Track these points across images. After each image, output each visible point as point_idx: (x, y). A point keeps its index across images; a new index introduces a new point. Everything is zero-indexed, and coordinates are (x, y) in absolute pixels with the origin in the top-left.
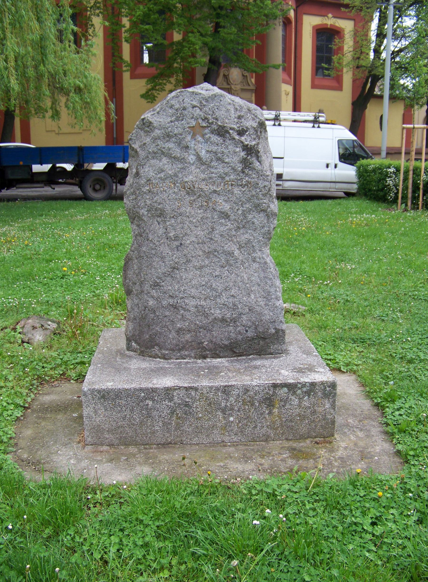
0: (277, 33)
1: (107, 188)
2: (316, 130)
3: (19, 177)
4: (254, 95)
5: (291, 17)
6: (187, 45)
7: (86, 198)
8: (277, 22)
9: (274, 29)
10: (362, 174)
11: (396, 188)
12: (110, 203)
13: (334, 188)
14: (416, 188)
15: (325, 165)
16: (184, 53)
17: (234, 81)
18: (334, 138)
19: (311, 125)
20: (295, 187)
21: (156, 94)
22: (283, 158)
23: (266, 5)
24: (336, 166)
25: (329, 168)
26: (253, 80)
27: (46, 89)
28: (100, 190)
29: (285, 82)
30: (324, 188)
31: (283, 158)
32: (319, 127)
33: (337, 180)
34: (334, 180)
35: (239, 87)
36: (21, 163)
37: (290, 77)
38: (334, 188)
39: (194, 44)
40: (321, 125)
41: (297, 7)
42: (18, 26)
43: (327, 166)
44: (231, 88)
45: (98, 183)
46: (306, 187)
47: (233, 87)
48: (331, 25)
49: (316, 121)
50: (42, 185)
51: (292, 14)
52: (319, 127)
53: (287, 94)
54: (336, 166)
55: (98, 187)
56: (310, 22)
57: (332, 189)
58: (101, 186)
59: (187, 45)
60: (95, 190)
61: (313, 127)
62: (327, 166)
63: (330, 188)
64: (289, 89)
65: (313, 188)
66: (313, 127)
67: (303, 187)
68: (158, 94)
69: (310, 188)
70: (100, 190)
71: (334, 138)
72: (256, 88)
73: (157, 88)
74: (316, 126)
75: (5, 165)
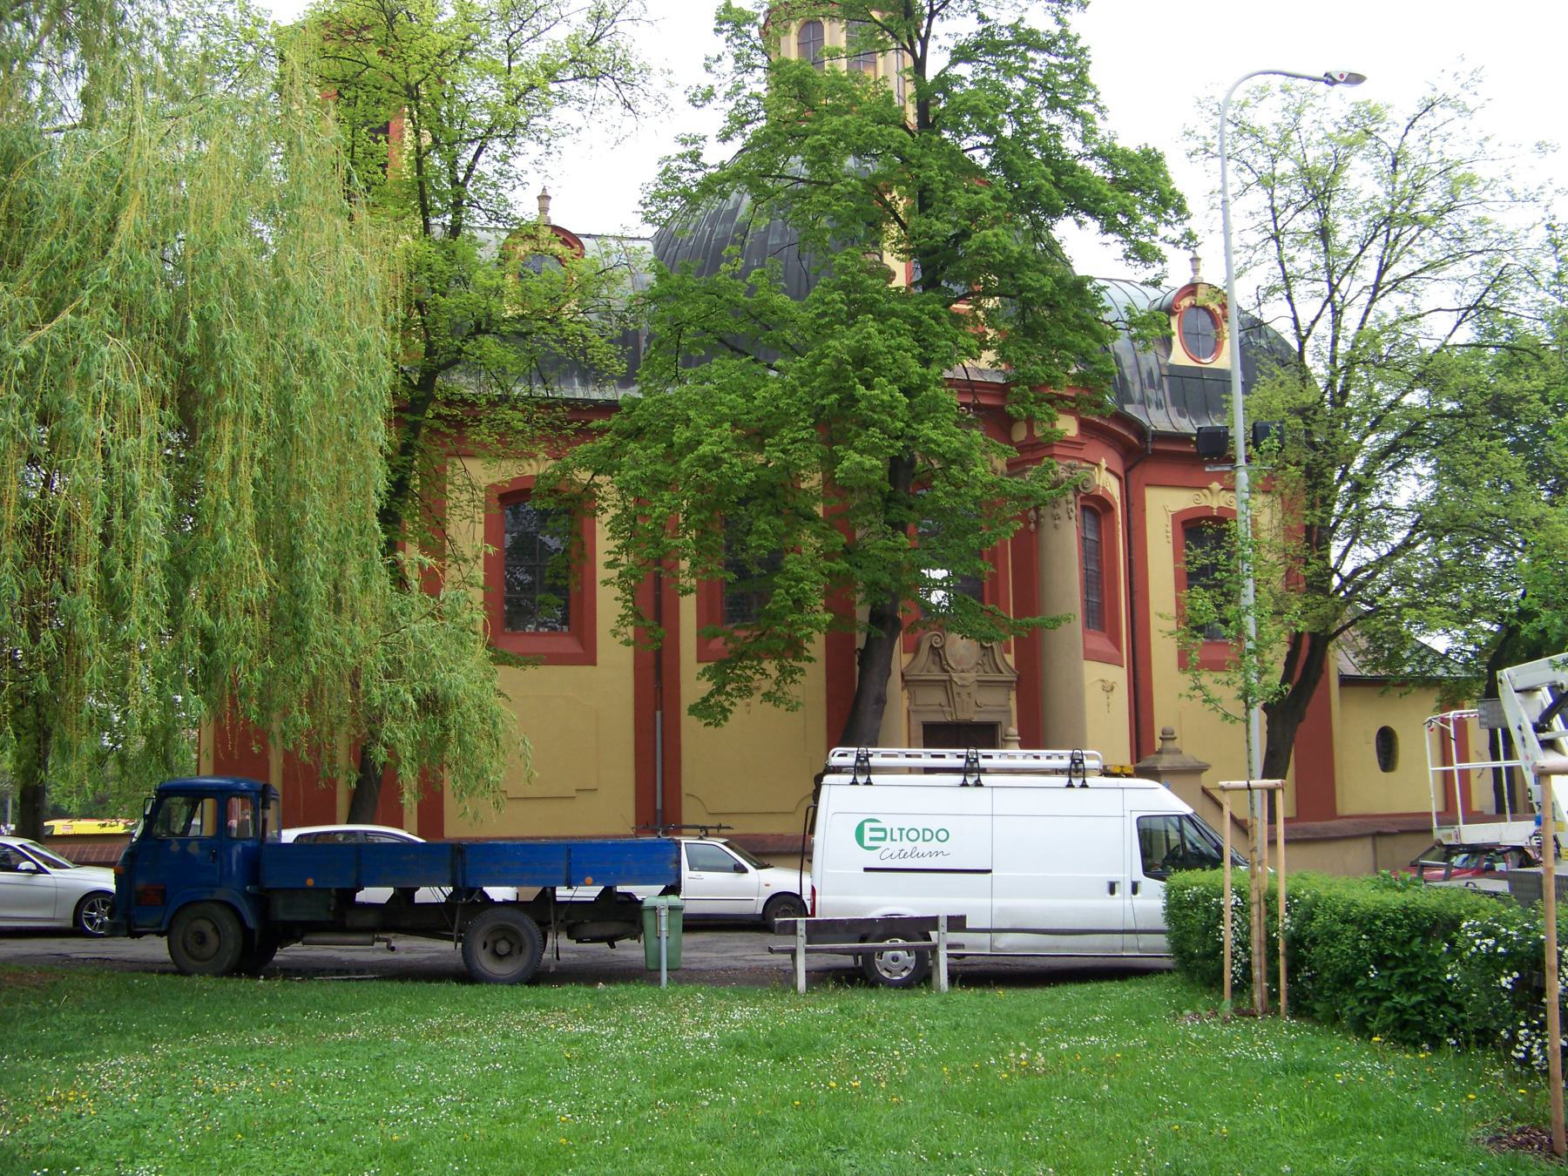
0: (1066, 540)
1: (527, 951)
2: (861, 790)
3: (306, 918)
4: (1013, 695)
5: (1112, 497)
6: (782, 582)
7: (467, 975)
8: (1061, 511)
9: (1056, 526)
10: (1177, 908)
11: (1245, 950)
12: (529, 994)
13: (1133, 949)
14: (1271, 945)
15: (1106, 887)
16: (776, 602)
17: (958, 663)
18: (1127, 813)
19: (1064, 780)
20: (1028, 948)
21: (726, 704)
22: (989, 871)
23: (975, 477)
24: (1135, 888)
25: (1117, 894)
26: (1010, 659)
27: (301, 712)
28: (509, 954)
29: (1090, 655)
30: (1104, 949)
31: (989, 871)
32: (869, 783)
33: (1141, 926)
34: (1132, 926)
35: (971, 677)
36: (310, 882)
37: (1118, 647)
38: (1133, 949)
39: (799, 580)
40: (984, 779)
41: (1127, 471)
42: (1527, 358)
43: (1112, 888)
44: (951, 680)
45: (504, 938)
46: (1058, 948)
47: (955, 677)
48: (1220, 508)
49: (1077, 771)
50: (368, 938)
51: (1108, 484)
52: (869, 783)
53: (1110, 689)
54: (1135, 888)
55: (503, 947)
56: (1164, 505)
57: (1127, 950)
58: (512, 945)
59: (782, 582)
60: (498, 956)
61: (1070, 785)
62: (1112, 888)
63: (1123, 949)
64: (1119, 676)
65: (1075, 949)
66: (1070, 785)
67: (1049, 948)
68: (732, 704)
69: (1068, 949)
70: (509, 954)
71: (1127, 813)
72: (1019, 677)
73: (728, 688)
74: (1077, 782)
75: (269, 885)
